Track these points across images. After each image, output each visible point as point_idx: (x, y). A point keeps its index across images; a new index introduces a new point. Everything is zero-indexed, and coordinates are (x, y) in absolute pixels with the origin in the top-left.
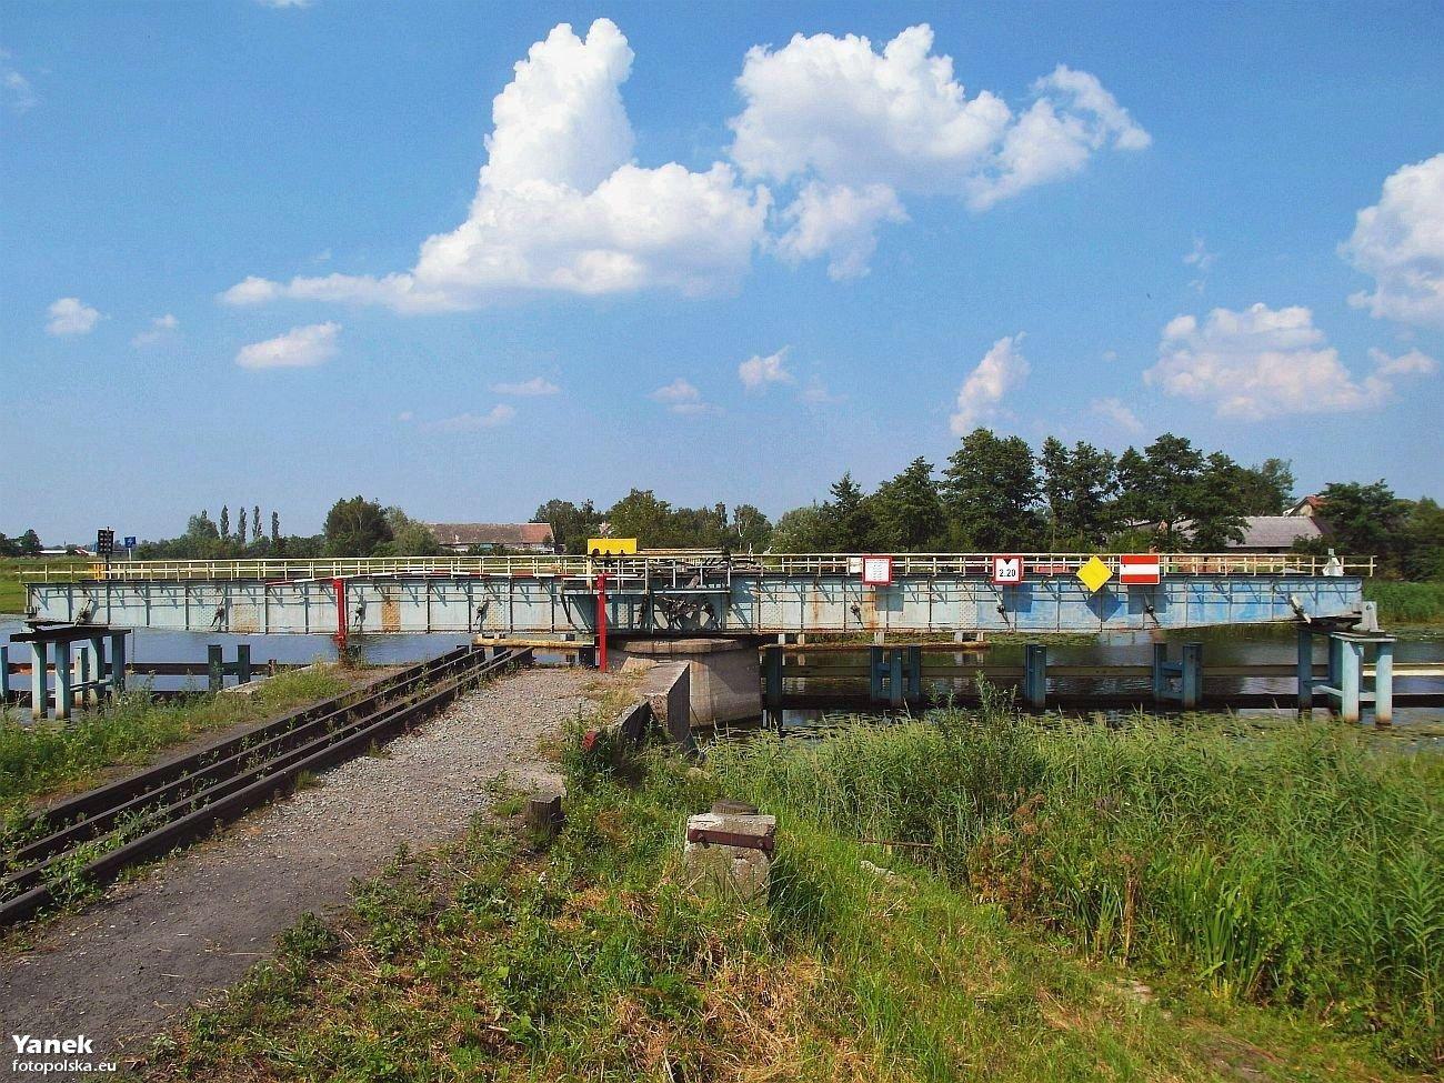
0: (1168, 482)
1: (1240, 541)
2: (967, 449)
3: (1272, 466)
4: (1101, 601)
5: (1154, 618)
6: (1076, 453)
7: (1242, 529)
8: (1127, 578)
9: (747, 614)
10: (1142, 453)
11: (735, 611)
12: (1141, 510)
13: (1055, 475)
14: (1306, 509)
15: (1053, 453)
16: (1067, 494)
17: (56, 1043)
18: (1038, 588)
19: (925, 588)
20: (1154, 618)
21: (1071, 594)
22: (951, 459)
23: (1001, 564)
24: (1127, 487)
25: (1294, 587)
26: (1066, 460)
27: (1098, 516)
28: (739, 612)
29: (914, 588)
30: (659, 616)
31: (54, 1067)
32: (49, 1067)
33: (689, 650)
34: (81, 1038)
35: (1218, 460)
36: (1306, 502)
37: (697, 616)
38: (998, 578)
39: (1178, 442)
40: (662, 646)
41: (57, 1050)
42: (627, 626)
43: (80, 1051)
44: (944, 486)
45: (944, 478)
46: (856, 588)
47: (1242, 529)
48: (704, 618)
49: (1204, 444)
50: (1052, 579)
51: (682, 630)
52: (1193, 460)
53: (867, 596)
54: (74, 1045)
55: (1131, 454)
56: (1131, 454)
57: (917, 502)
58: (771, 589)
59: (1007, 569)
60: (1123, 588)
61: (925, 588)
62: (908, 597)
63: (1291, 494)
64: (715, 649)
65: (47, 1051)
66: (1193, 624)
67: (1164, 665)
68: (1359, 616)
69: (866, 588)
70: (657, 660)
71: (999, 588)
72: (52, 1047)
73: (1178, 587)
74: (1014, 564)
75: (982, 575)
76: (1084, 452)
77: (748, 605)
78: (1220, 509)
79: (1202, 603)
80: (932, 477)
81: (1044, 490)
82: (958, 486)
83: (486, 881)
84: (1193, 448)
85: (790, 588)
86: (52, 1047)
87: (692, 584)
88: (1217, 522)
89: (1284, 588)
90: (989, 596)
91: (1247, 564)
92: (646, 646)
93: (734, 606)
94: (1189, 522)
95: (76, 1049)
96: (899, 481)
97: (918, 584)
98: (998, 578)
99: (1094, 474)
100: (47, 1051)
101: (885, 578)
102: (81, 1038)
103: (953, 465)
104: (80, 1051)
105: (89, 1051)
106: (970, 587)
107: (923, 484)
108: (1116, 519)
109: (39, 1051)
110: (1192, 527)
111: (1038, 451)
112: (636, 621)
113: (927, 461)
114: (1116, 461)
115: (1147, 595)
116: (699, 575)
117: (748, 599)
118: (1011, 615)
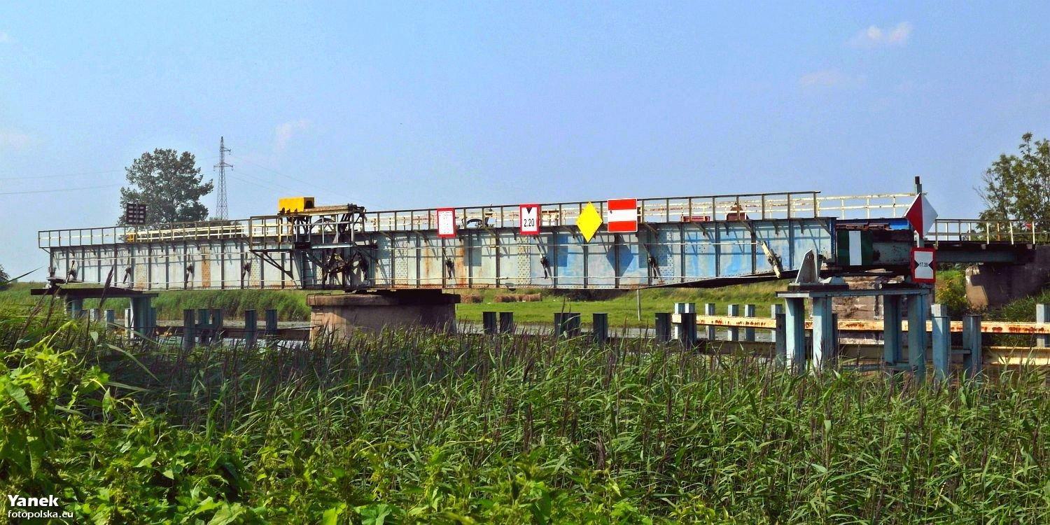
17: (35, 500)
34: (51, 496)
41: (36, 505)
54: (47, 501)
65: (30, 505)
72: (33, 502)
100: (30, 505)
102: (51, 496)
109: (24, 505)
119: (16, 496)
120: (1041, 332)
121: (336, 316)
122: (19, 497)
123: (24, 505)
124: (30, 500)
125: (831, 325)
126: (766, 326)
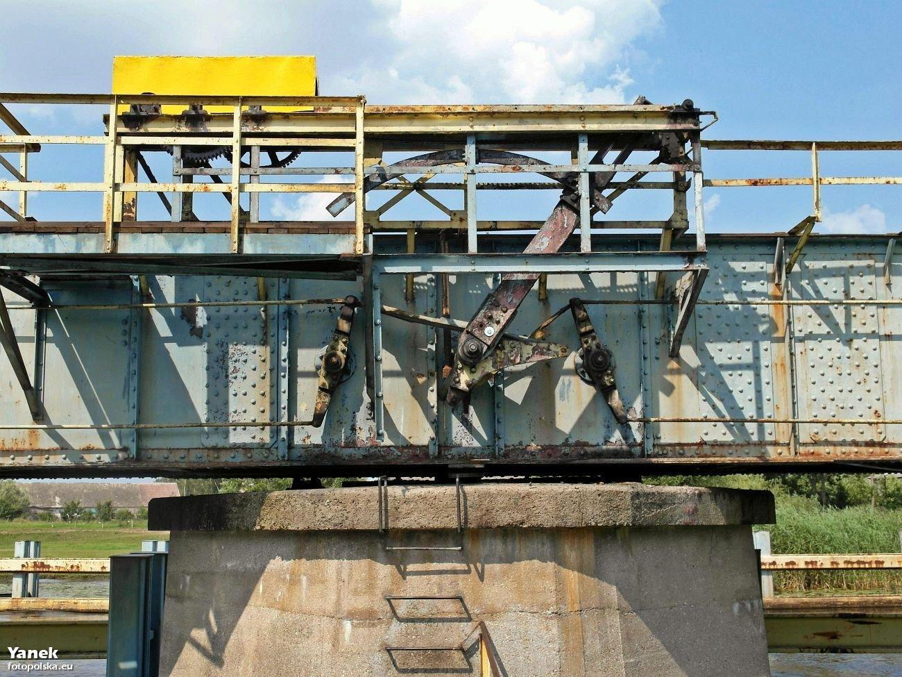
9: (741, 384)
11: (694, 375)
17: (35, 652)
28: (709, 379)
30: (395, 391)
31: (34, 667)
32: (30, 667)
33: (546, 519)
34: (51, 649)
37: (543, 394)
40: (424, 504)
41: (36, 657)
42: (266, 436)
48: (573, 400)
51: (490, 447)
54: (46, 653)
58: (831, 288)
64: (648, 515)
65: (29, 657)
70: (399, 562)
72: (33, 654)
77: (738, 351)
83: (405, 505)
86: (33, 654)
92: (352, 503)
93: (687, 352)
95: (48, 656)
97: (845, 273)
100: (29, 657)
102: (51, 649)
109: (24, 657)
112: (305, 410)
117: (744, 326)
119: (16, 649)
120: (772, 567)
121: (573, 576)
122: (19, 649)
123: (24, 657)
124: (30, 652)
125: (91, 608)
126: (885, 565)
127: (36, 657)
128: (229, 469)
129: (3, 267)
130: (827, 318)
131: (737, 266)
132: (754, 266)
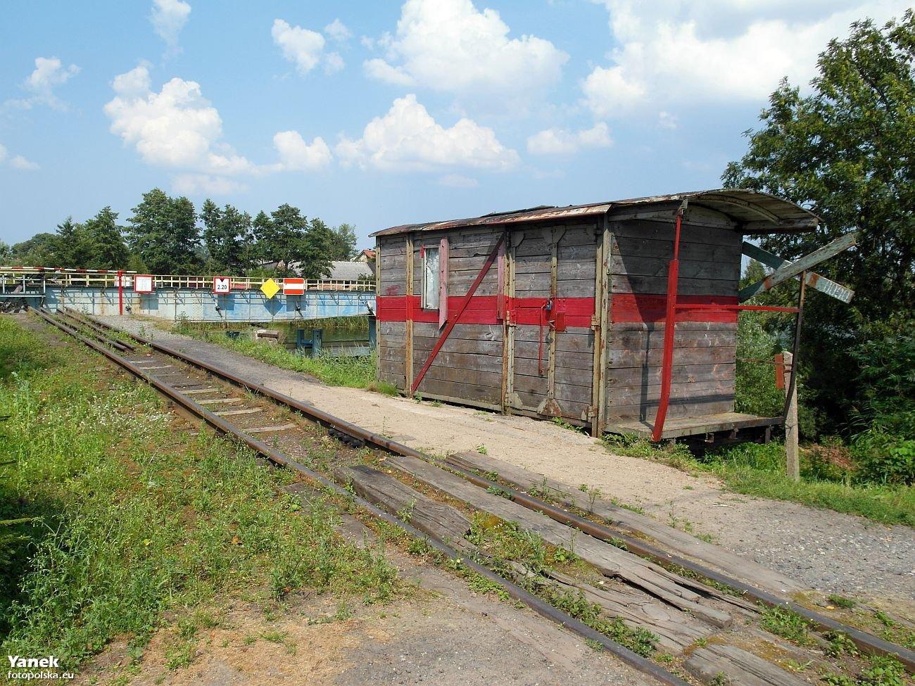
0: (286, 236)
1: (329, 276)
2: (147, 203)
3: (344, 229)
4: (272, 304)
5: (300, 314)
6: (225, 213)
7: (330, 268)
8: (287, 291)
10: (269, 215)
12: (268, 255)
13: (211, 227)
14: (363, 257)
15: (210, 212)
16: (219, 241)
17: (36, 661)
18: (238, 296)
19: (172, 295)
20: (300, 314)
21: (257, 300)
22: (135, 211)
23: (218, 281)
24: (259, 238)
25: (368, 297)
26: (219, 216)
27: (241, 257)
29: (165, 295)
34: (51, 658)
35: (318, 225)
36: (363, 253)
38: (217, 290)
39: (293, 210)
41: (36, 665)
43: (51, 666)
44: (128, 230)
45: (130, 224)
46: (129, 295)
47: (330, 268)
49: (309, 213)
50: (246, 291)
52: (301, 223)
53: (136, 301)
54: (47, 662)
55: (262, 216)
56: (262, 216)
57: (105, 240)
58: (71, 295)
59: (222, 285)
60: (284, 297)
61: (172, 295)
62: (161, 301)
63: (356, 248)
65: (30, 665)
66: (320, 317)
67: (303, 341)
68: (680, 306)
69: (135, 295)
71: (216, 296)
72: (33, 663)
73: (312, 296)
74: (226, 281)
75: (209, 288)
76: (230, 212)
78: (318, 255)
79: (324, 305)
80: (117, 222)
81: (203, 238)
82: (138, 230)
84: (301, 215)
85: (85, 295)
86: (33, 663)
87: (17, 291)
88: (314, 264)
89: (363, 297)
90: (210, 301)
91: (331, 286)
94: (298, 264)
95: (48, 664)
96: (90, 224)
98: (217, 290)
99: (237, 228)
100: (30, 665)
101: (149, 289)
102: (51, 658)
103: (135, 215)
104: (51, 666)
105: (56, 665)
106: (199, 295)
107: (110, 228)
108: (252, 259)
110: (300, 267)
111: (199, 210)
113: (112, 211)
114: (253, 220)
115: (297, 300)
116: (22, 285)
118: (223, 312)
119: (17, 657)
127: (36, 665)
128: (508, 27)
129: (2, 522)
130: (70, 300)
131: (54, 291)
132: (58, 291)
